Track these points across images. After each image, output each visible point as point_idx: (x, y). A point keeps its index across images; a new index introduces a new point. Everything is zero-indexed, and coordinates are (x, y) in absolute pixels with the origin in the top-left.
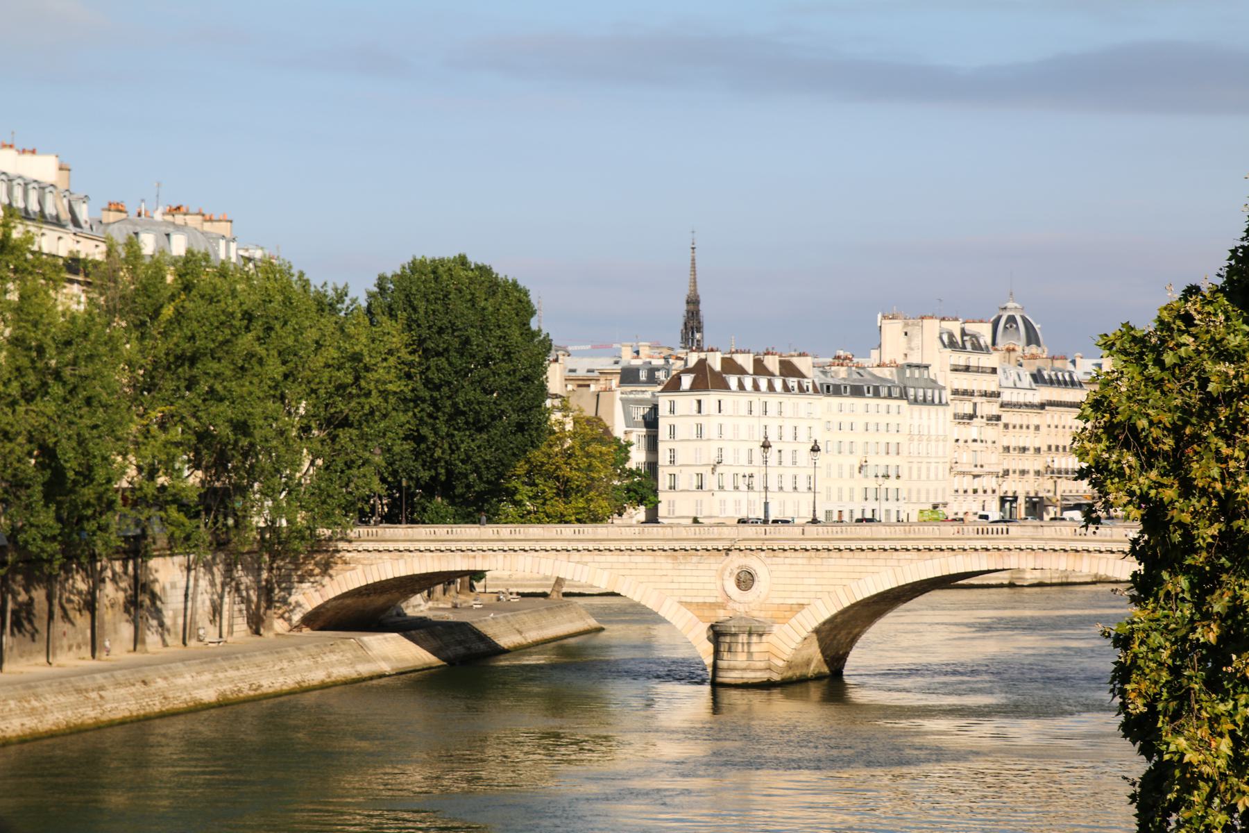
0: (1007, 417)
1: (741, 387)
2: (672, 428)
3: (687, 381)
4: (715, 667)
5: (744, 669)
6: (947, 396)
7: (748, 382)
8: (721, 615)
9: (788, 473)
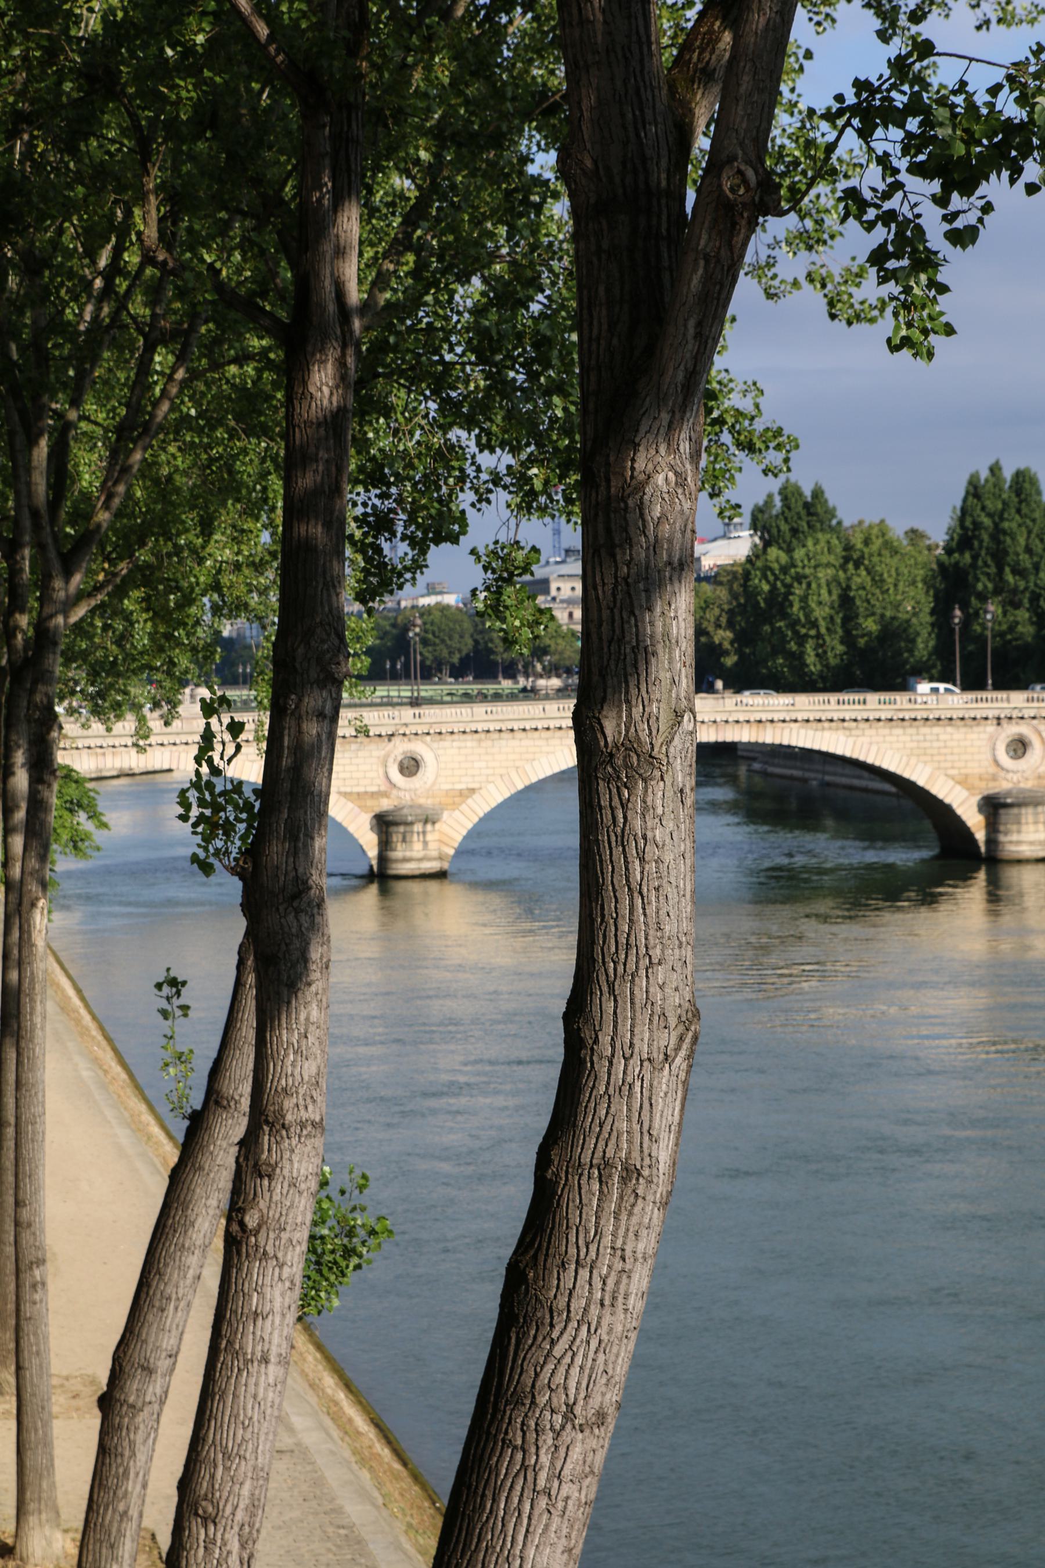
5: (420, 860)
8: (385, 805)
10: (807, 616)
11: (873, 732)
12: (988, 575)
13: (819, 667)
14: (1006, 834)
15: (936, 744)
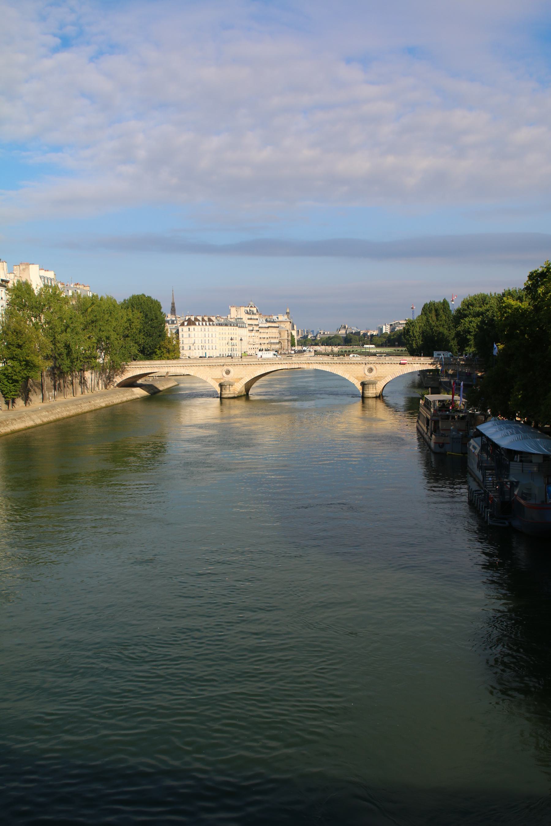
0: (261, 330)
1: (199, 324)
2: (183, 335)
3: (186, 323)
4: (221, 394)
6: (247, 325)
7: (201, 323)
8: (222, 381)
9: (211, 345)
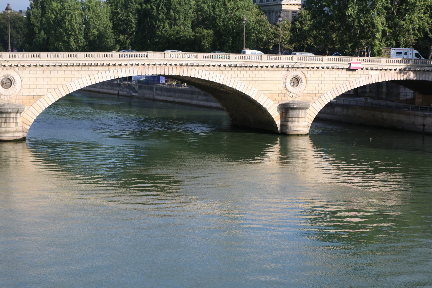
5: (14, 132)
10: (71, 28)
11: (232, 72)
12: (163, 12)
13: (75, 47)
14: (292, 122)
15: (260, 79)
